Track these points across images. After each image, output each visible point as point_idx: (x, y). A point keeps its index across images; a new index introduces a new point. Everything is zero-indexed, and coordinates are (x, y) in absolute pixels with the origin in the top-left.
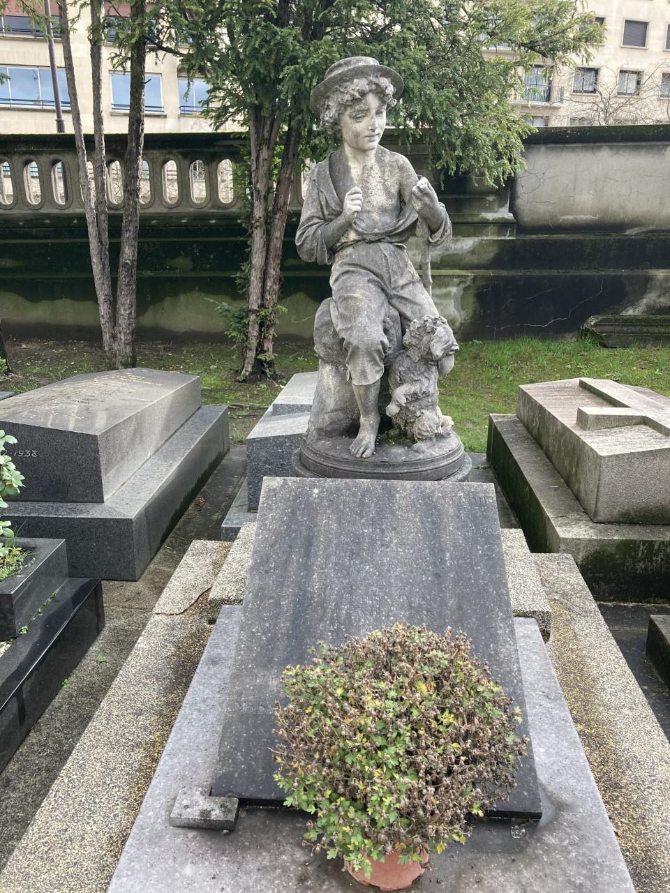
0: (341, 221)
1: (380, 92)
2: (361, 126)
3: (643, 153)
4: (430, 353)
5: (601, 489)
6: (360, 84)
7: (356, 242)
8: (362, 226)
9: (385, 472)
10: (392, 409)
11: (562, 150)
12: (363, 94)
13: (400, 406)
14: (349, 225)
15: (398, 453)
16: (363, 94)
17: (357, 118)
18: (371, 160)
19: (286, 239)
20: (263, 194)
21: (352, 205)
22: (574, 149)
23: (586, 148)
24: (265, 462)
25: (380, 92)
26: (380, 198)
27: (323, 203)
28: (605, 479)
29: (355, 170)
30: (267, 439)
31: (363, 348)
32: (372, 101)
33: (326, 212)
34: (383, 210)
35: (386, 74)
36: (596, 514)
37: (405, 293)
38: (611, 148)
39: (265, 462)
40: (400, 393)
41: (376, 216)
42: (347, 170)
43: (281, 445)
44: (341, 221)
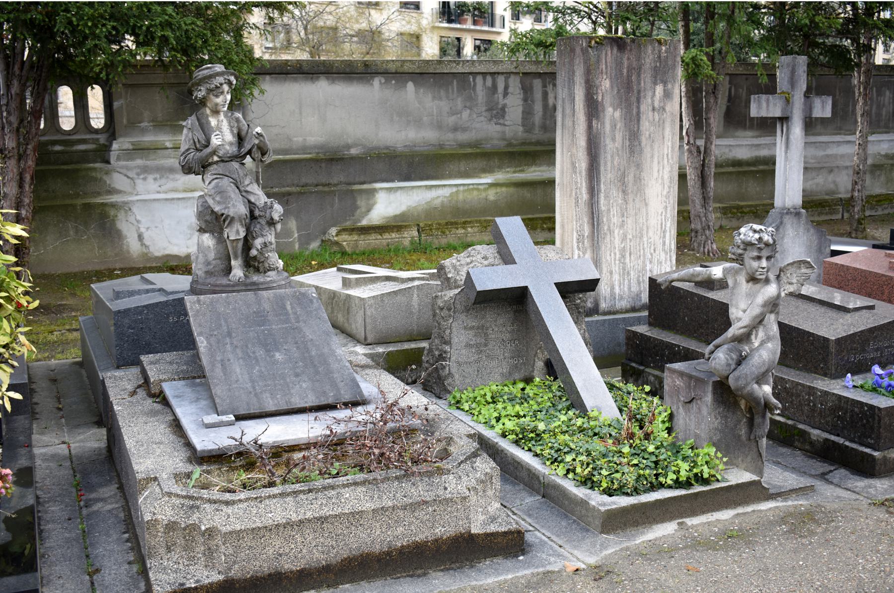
0: (208, 150)
1: (230, 83)
2: (219, 100)
3: (355, 82)
4: (272, 219)
5: (367, 321)
6: (221, 79)
7: (217, 162)
8: (221, 153)
9: (255, 287)
10: (254, 252)
11: (285, 80)
12: (221, 84)
13: (258, 250)
14: (214, 153)
15: (256, 278)
16: (221, 84)
17: (217, 96)
18: (222, 117)
19: (39, 168)
20: (15, 125)
21: (215, 141)
22: (295, 80)
23: (306, 79)
24: (129, 328)
25: (230, 83)
26: (229, 137)
27: (196, 140)
28: (368, 313)
29: (213, 122)
30: (129, 309)
31: (236, 217)
32: (226, 88)
33: (198, 146)
34: (231, 144)
35: (232, 74)
36: (366, 339)
37: (248, 189)
38: (328, 79)
39: (129, 328)
40: (258, 242)
41: (228, 147)
42: (209, 123)
43: (141, 313)
44: (208, 150)
